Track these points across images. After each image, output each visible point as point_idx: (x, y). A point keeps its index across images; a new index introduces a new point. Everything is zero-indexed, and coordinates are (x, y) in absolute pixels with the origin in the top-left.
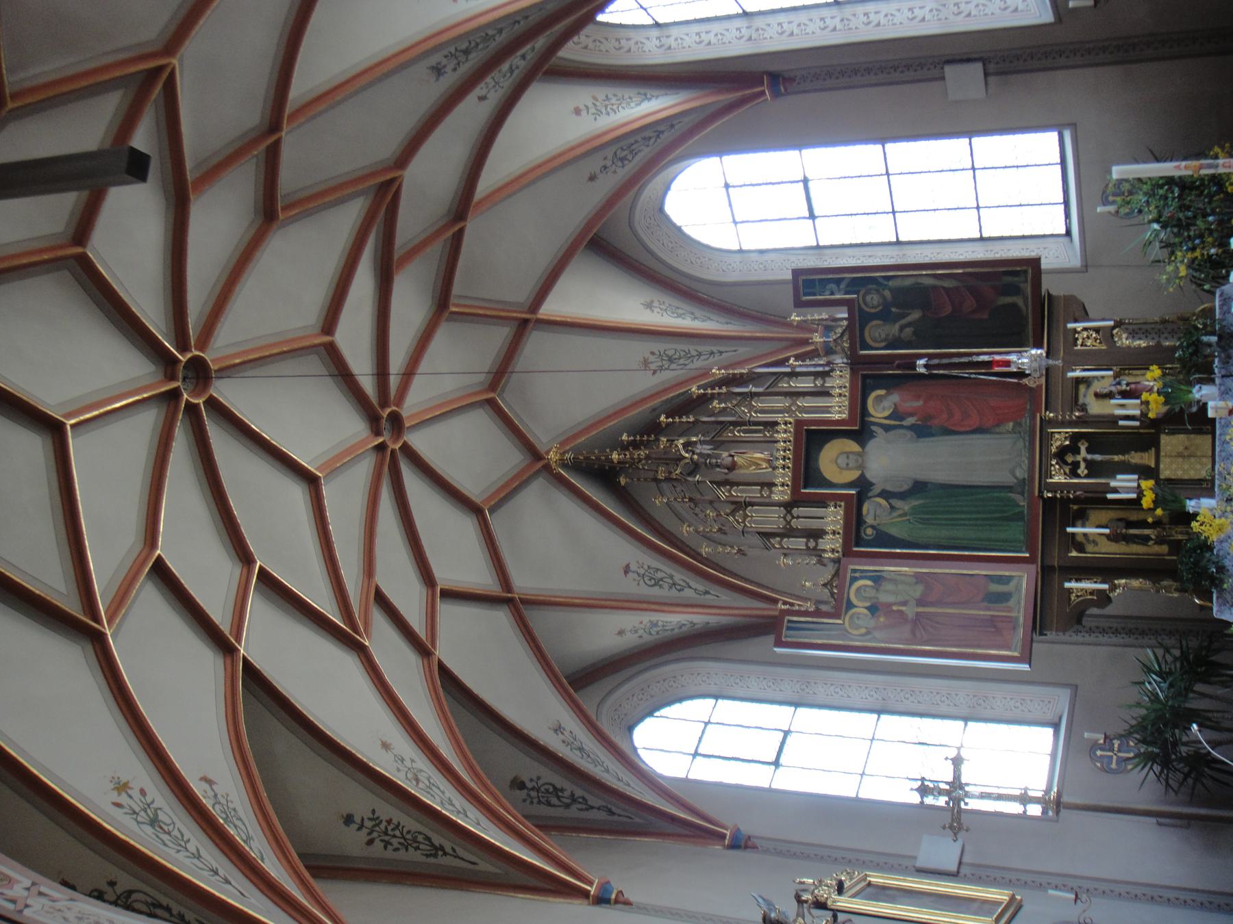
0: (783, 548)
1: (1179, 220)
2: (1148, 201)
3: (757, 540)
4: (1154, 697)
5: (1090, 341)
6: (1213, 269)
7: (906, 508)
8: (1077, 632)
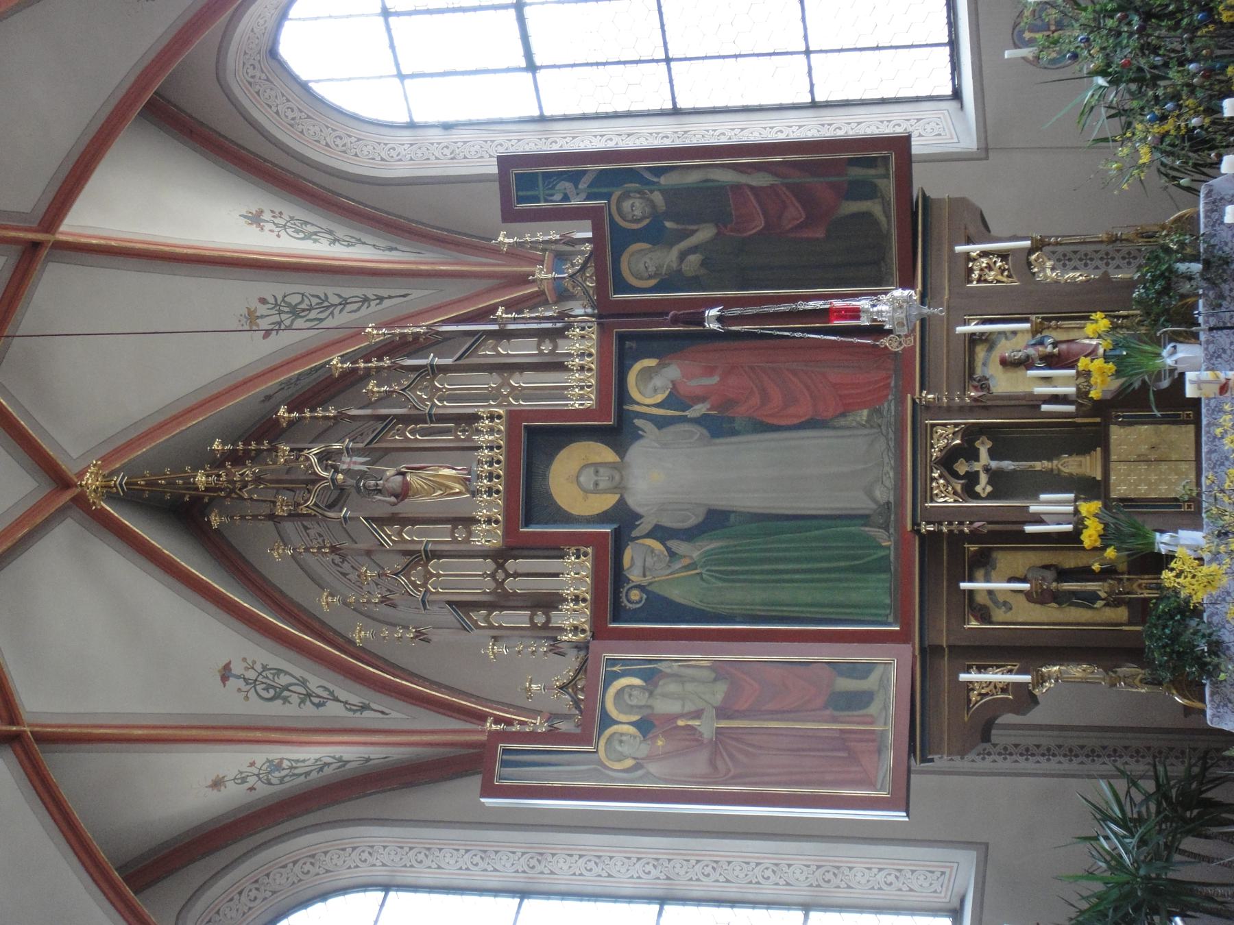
0: (491, 627)
1: (1140, 69)
2: (1088, 40)
3: (448, 616)
4: (1116, 863)
5: (992, 273)
6: (1195, 152)
7: (696, 554)
8: (985, 754)
